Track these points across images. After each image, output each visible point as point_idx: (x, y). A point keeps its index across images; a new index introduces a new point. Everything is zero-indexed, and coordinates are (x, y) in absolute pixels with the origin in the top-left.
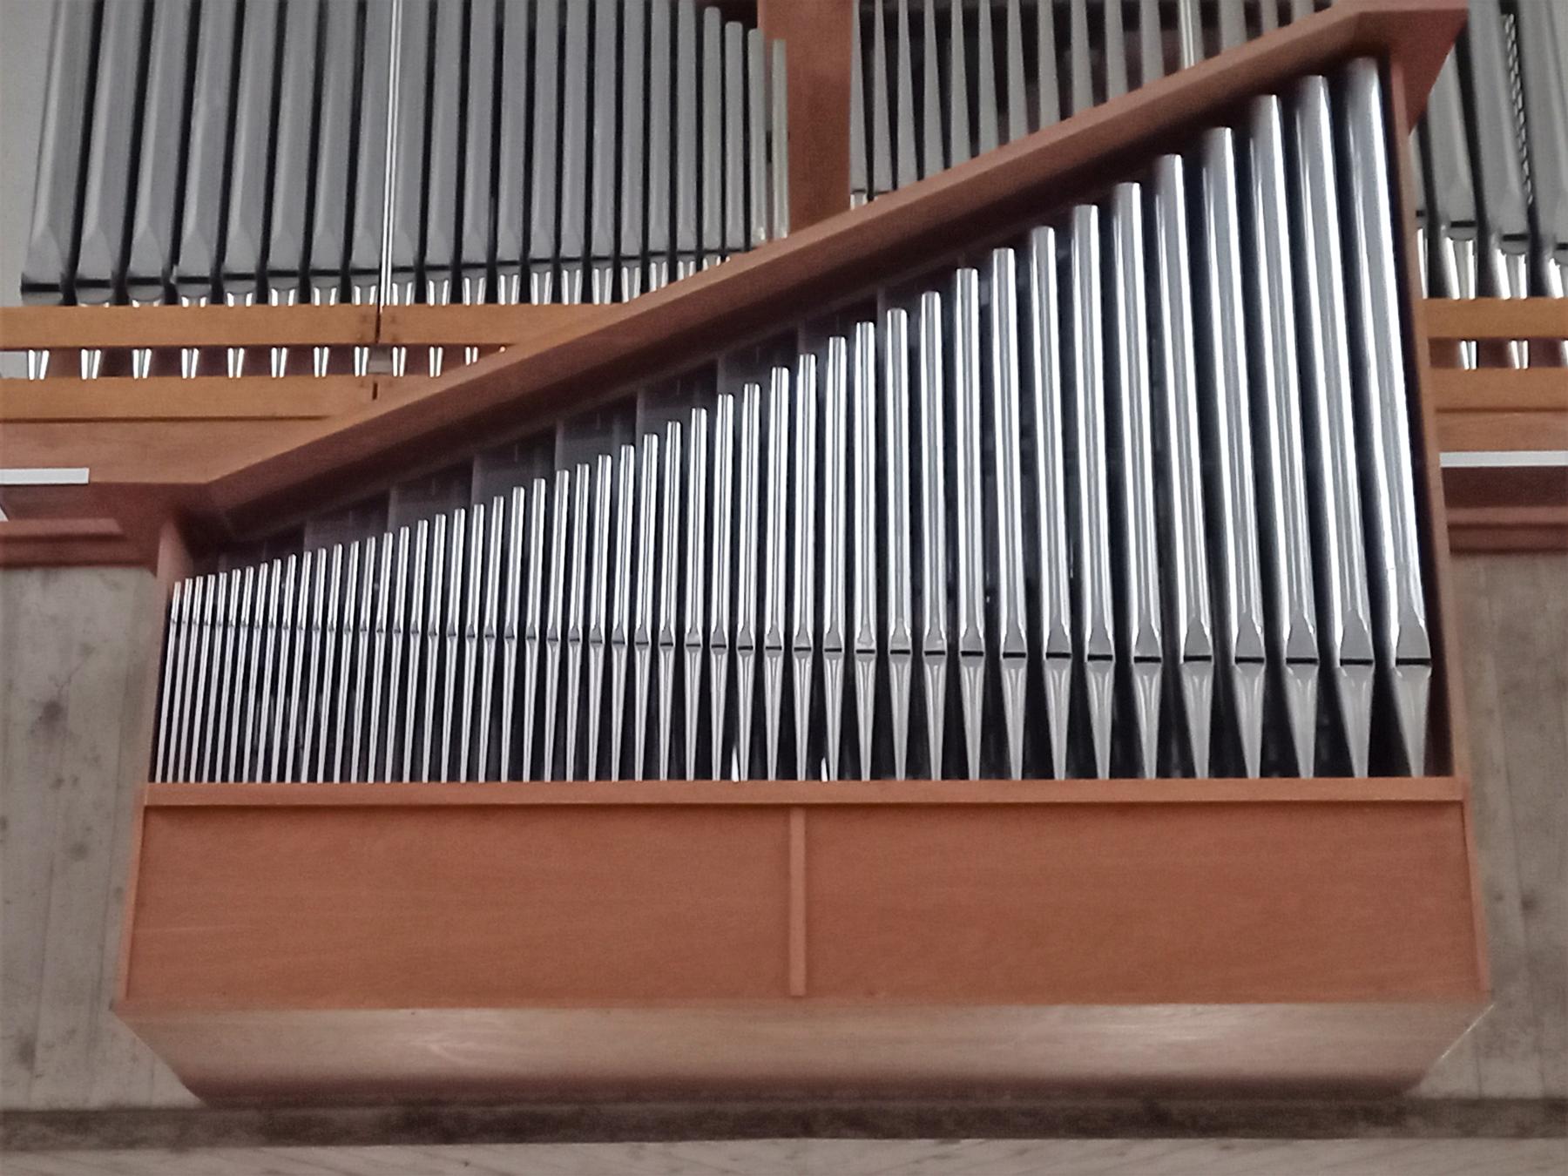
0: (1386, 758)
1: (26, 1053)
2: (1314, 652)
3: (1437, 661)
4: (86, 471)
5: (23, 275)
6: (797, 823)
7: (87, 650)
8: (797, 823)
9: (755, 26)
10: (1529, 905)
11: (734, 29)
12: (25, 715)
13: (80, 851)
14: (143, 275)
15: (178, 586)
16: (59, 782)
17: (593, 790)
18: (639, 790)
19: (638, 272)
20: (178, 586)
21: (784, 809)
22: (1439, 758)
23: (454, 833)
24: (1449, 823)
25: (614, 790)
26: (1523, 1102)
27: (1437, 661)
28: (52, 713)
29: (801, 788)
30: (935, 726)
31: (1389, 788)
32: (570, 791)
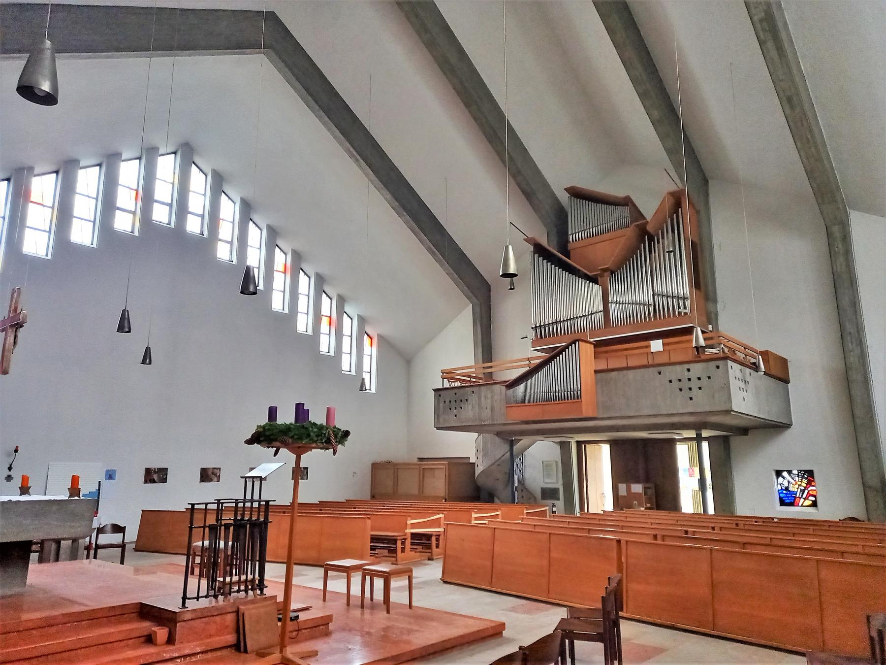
4: (625, 494)
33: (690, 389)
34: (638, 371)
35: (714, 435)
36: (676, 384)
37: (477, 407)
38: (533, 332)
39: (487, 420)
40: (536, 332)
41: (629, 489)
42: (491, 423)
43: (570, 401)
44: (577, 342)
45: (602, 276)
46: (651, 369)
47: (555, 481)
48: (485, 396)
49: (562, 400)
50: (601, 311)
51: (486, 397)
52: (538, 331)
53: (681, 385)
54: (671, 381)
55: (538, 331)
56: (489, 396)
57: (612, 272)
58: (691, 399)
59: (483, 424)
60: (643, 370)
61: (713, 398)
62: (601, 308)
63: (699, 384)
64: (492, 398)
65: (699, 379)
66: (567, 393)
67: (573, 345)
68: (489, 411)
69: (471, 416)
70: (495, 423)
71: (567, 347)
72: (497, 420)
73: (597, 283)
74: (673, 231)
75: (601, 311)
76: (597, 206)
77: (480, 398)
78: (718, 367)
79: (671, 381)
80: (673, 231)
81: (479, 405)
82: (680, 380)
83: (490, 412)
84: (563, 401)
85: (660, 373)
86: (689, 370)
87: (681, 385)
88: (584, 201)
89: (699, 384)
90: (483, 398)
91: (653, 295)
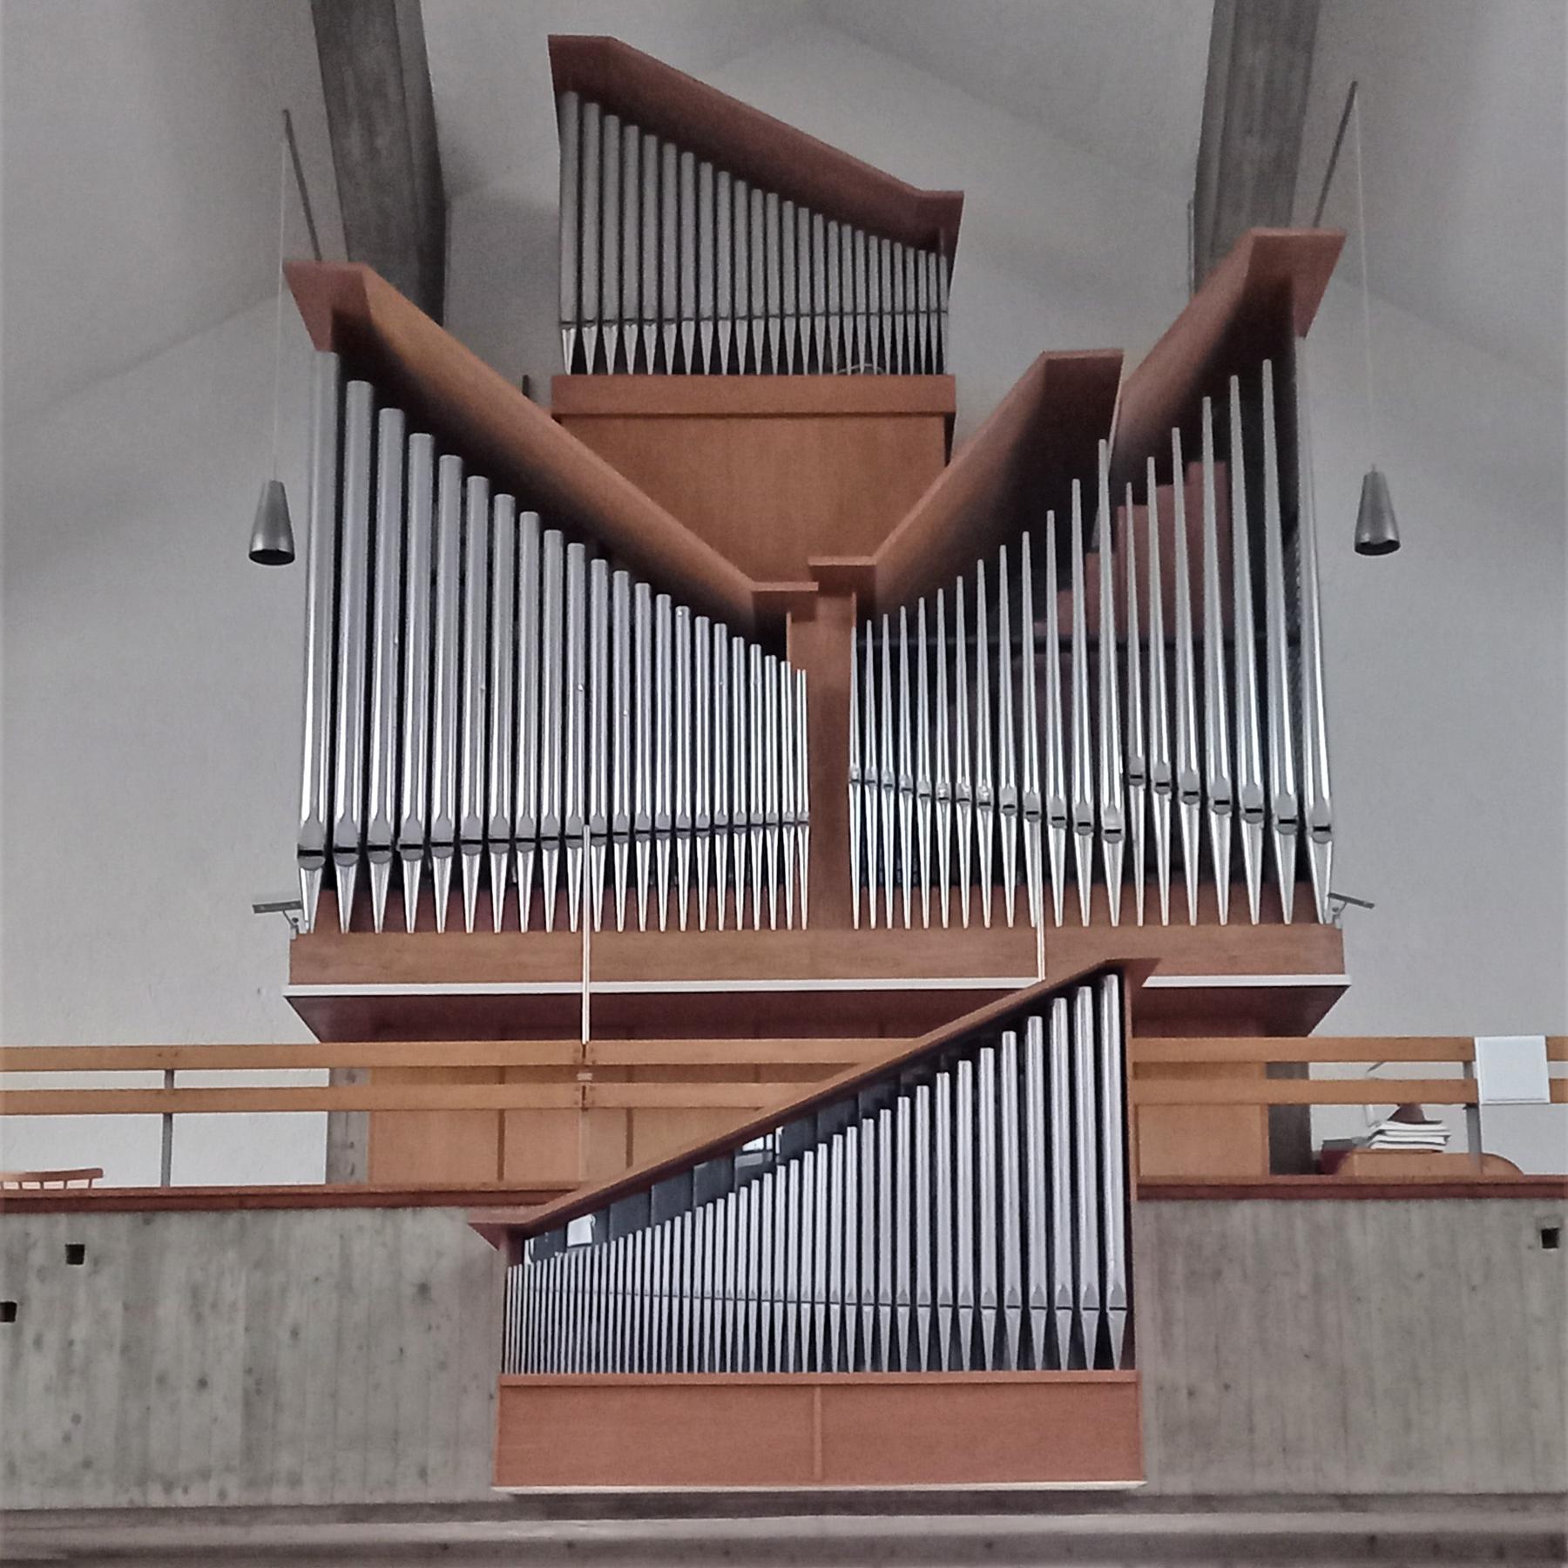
0: (1104, 1360)
1: (423, 1473)
3: (1130, 1310)
5: (299, 846)
6: (818, 1390)
7: (440, 1254)
8: (818, 1390)
9: (785, 659)
10: (1191, 1393)
11: (771, 660)
12: (409, 1291)
13: (443, 1366)
14: (378, 843)
15: (510, 1269)
16: (430, 1328)
17: (719, 1378)
18: (740, 1377)
19: (707, 840)
20: (510, 1269)
21: (812, 1386)
22: (1129, 1359)
23: (652, 1399)
24: (1130, 1392)
25: (728, 1377)
26: (1184, 1497)
27: (1130, 1310)
28: (423, 1289)
29: (820, 1376)
30: (942, 677)
31: (1105, 1375)
32: (707, 1378)
34: (1416, 1213)
35: (18, 1557)
37: (109, 1366)
38: (308, 884)
39: (205, 1475)
40: (329, 882)
42: (236, 1495)
43: (1039, 1373)
44: (1114, 979)
45: (804, 609)
46: (1495, 1209)
48: (195, 1293)
49: (894, 1365)
50: (797, 823)
51: (198, 1302)
52: (346, 880)
55: (346, 880)
56: (235, 1290)
57: (867, 612)
59: (157, 1498)
60: (1442, 1210)
62: (798, 798)
64: (262, 1305)
67: (1086, 994)
68: (224, 1403)
69: (47, 1435)
70: (280, 1495)
71: (1040, 1005)
72: (295, 1481)
73: (774, 645)
74: (1222, 453)
75: (797, 823)
76: (765, 199)
77: (139, 1307)
80: (1222, 453)
81: (133, 1351)
83: (233, 1418)
88: (670, 151)
91: (1126, 780)
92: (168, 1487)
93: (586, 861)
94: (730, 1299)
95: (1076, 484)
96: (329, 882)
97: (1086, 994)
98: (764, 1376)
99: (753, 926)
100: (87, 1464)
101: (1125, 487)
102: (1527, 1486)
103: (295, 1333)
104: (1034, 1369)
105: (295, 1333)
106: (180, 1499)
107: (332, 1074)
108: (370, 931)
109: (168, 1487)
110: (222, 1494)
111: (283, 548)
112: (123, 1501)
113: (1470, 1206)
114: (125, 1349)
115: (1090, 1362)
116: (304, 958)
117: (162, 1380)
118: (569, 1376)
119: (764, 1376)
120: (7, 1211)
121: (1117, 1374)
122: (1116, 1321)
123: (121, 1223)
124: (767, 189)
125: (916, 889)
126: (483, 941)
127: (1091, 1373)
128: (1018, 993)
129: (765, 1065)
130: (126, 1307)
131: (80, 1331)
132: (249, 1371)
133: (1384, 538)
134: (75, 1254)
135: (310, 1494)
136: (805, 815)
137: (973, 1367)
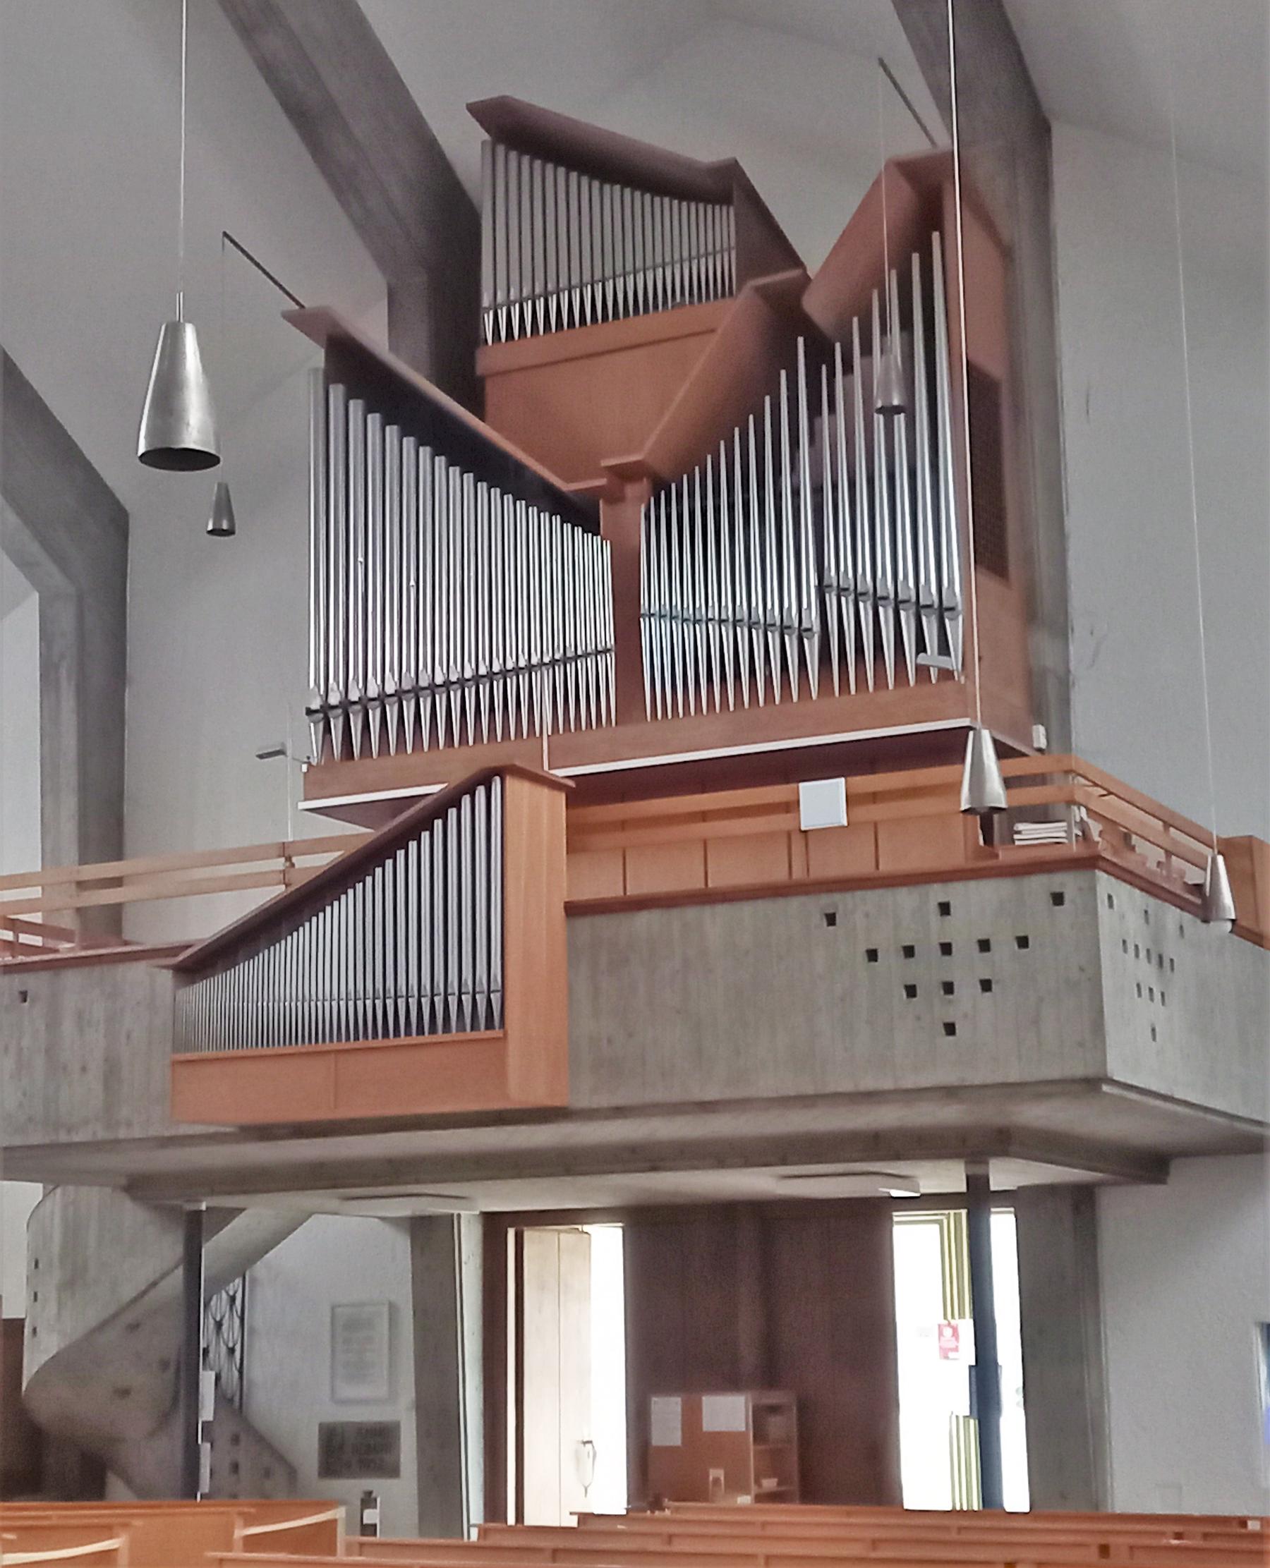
2: (499, 988)
10: (609, 1041)
33: (948, 988)
36: (890, 959)
37: (40, 1061)
38: (314, 732)
40: (327, 730)
41: (692, 1417)
42: (102, 1134)
44: (498, 779)
45: (615, 498)
46: (795, 904)
47: (383, 1391)
48: (80, 1016)
50: (606, 651)
53: (916, 971)
54: (872, 955)
57: (659, 486)
58: (950, 1029)
59: (63, 1137)
61: (1036, 1022)
63: (982, 966)
65: (984, 945)
66: (460, 1001)
67: (481, 791)
70: (122, 1134)
72: (129, 1125)
73: (592, 527)
74: (907, 324)
75: (606, 651)
77: (53, 1023)
78: (1058, 899)
79: (872, 955)
80: (907, 324)
81: (51, 1051)
82: (909, 951)
84: (415, 1039)
85: (831, 919)
86: (945, 909)
87: (916, 971)
89: (982, 966)
90: (68, 1026)
91: (822, 589)
92: (69, 1131)
93: (543, 682)
94: (482, 992)
95: (783, 373)
96: (327, 730)
97: (481, 791)
98: (352, 1044)
99: (468, 742)
100: (30, 1119)
101: (821, 368)
102: (810, 1090)
103: (128, 1037)
104: (479, 1030)
105: (128, 1037)
106: (77, 1138)
107: (43, 889)
108: (368, 757)
109: (69, 1131)
110: (94, 1133)
111: (225, 526)
112: (47, 1140)
113: (781, 902)
114: (47, 1051)
115: (468, 1027)
116: (315, 782)
117: (65, 1068)
118: (206, 1054)
119: (352, 1044)
120: (5, 973)
121: (497, 1033)
122: (495, 998)
123: (44, 976)
124: (613, 182)
125: (785, 672)
126: (385, 762)
127: (483, 1033)
128: (430, 797)
129: (880, 792)
130: (47, 1025)
131: (26, 1042)
132: (106, 1060)
133: (891, 403)
134: (24, 996)
135: (137, 1133)
136: (611, 643)
137: (418, 1034)
